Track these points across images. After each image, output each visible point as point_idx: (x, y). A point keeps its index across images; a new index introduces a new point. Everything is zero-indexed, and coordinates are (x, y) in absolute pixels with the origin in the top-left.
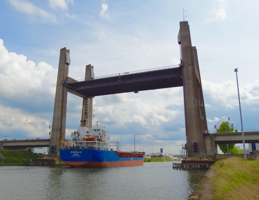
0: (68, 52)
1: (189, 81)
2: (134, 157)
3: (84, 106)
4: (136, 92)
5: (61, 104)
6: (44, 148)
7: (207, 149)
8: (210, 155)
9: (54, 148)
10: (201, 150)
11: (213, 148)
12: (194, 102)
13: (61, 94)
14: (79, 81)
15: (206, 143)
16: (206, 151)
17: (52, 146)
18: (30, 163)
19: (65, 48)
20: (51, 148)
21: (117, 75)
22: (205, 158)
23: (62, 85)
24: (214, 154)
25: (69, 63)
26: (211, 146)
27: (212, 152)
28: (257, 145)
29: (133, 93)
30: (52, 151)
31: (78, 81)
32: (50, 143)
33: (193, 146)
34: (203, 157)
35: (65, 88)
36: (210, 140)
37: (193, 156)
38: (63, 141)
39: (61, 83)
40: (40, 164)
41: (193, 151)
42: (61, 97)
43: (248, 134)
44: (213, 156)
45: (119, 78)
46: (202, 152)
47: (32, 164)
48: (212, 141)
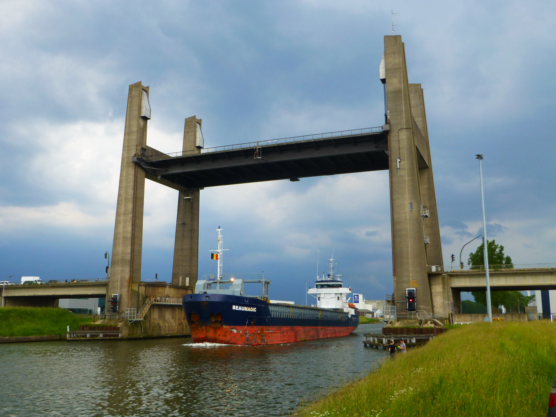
0: (146, 92)
1: (402, 163)
2: (322, 325)
3: (124, 152)
4: (294, 178)
5: (130, 206)
6: (90, 299)
7: (435, 304)
8: (441, 316)
9: (116, 302)
10: (422, 307)
11: (447, 302)
12: (412, 207)
13: (132, 184)
14: (173, 156)
15: (433, 291)
16: (433, 307)
17: (112, 298)
18: (68, 336)
19: (138, 85)
20: (110, 302)
21: (252, 145)
22: (429, 322)
23: (132, 165)
24: (449, 315)
25: (149, 117)
26: (444, 298)
27: (444, 310)
28: (551, 293)
29: (285, 182)
30: (112, 308)
31: (170, 155)
32: (107, 291)
33: (406, 297)
34: (426, 322)
35: (141, 173)
36: (441, 286)
37: (406, 319)
38: (137, 286)
39: (131, 161)
40: (88, 336)
41: (407, 309)
42: (131, 192)
43: (516, 273)
44: (446, 319)
45: (257, 151)
46: (424, 309)
47: (70, 337)
48: (446, 286)
